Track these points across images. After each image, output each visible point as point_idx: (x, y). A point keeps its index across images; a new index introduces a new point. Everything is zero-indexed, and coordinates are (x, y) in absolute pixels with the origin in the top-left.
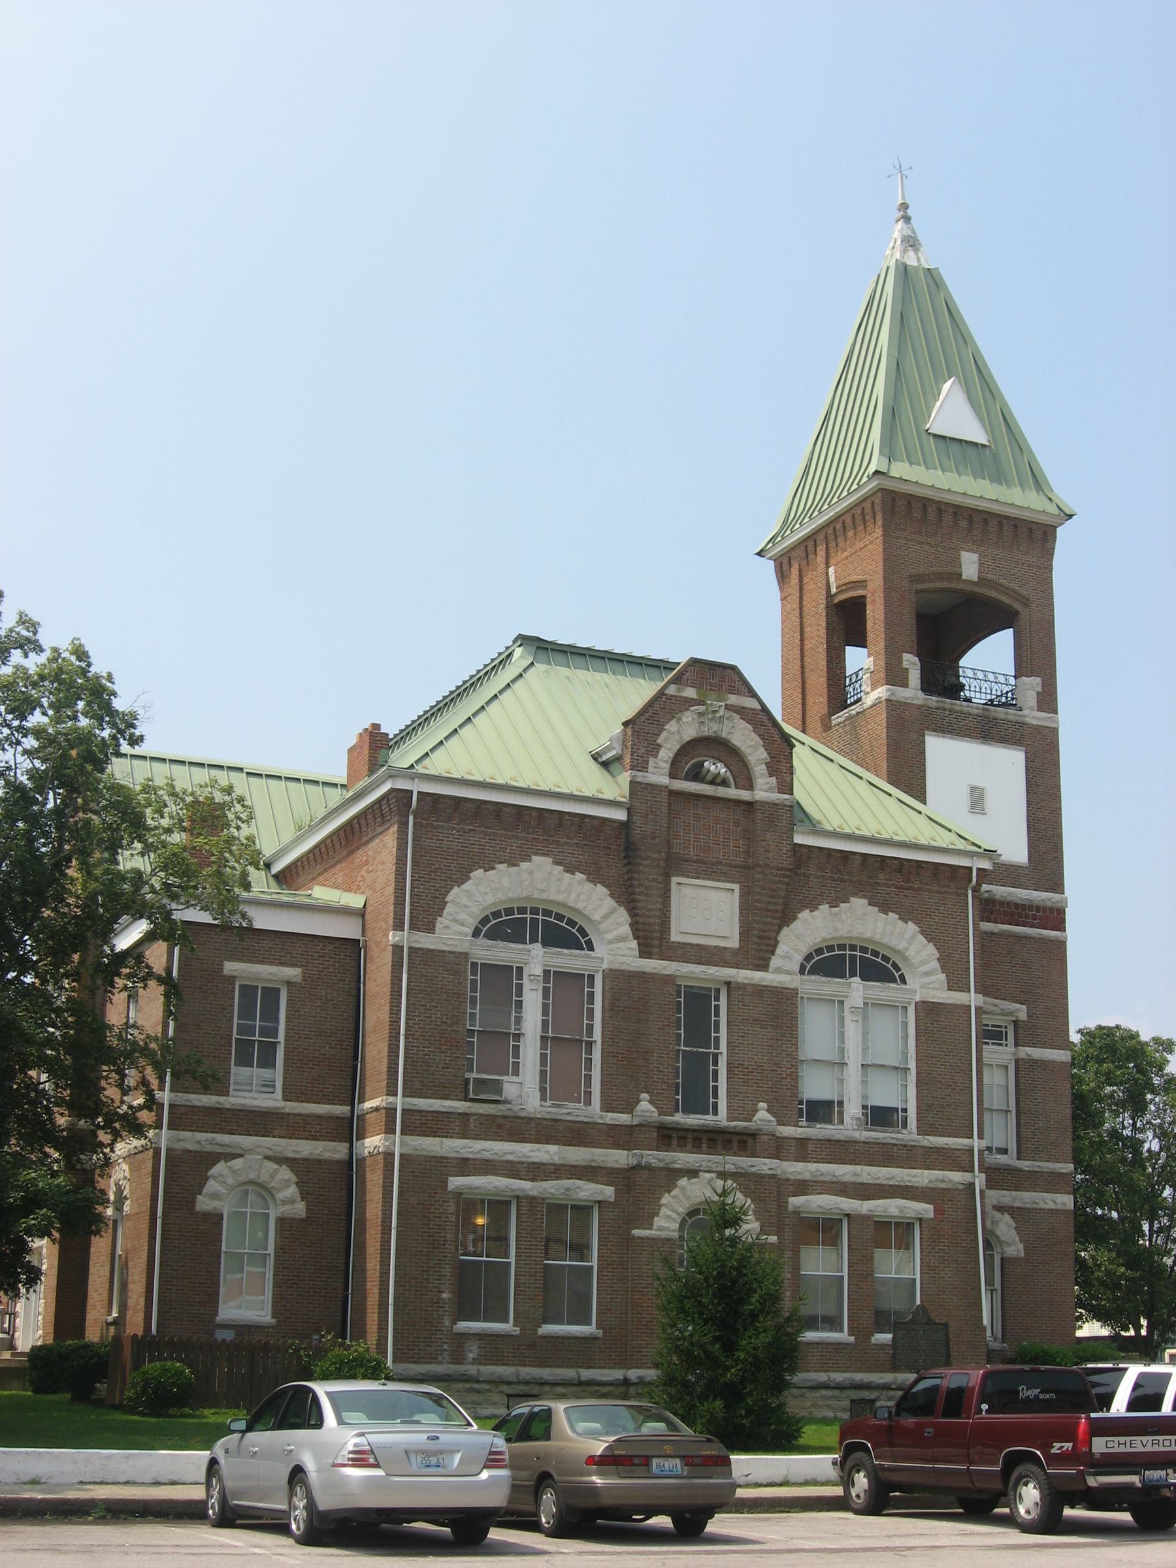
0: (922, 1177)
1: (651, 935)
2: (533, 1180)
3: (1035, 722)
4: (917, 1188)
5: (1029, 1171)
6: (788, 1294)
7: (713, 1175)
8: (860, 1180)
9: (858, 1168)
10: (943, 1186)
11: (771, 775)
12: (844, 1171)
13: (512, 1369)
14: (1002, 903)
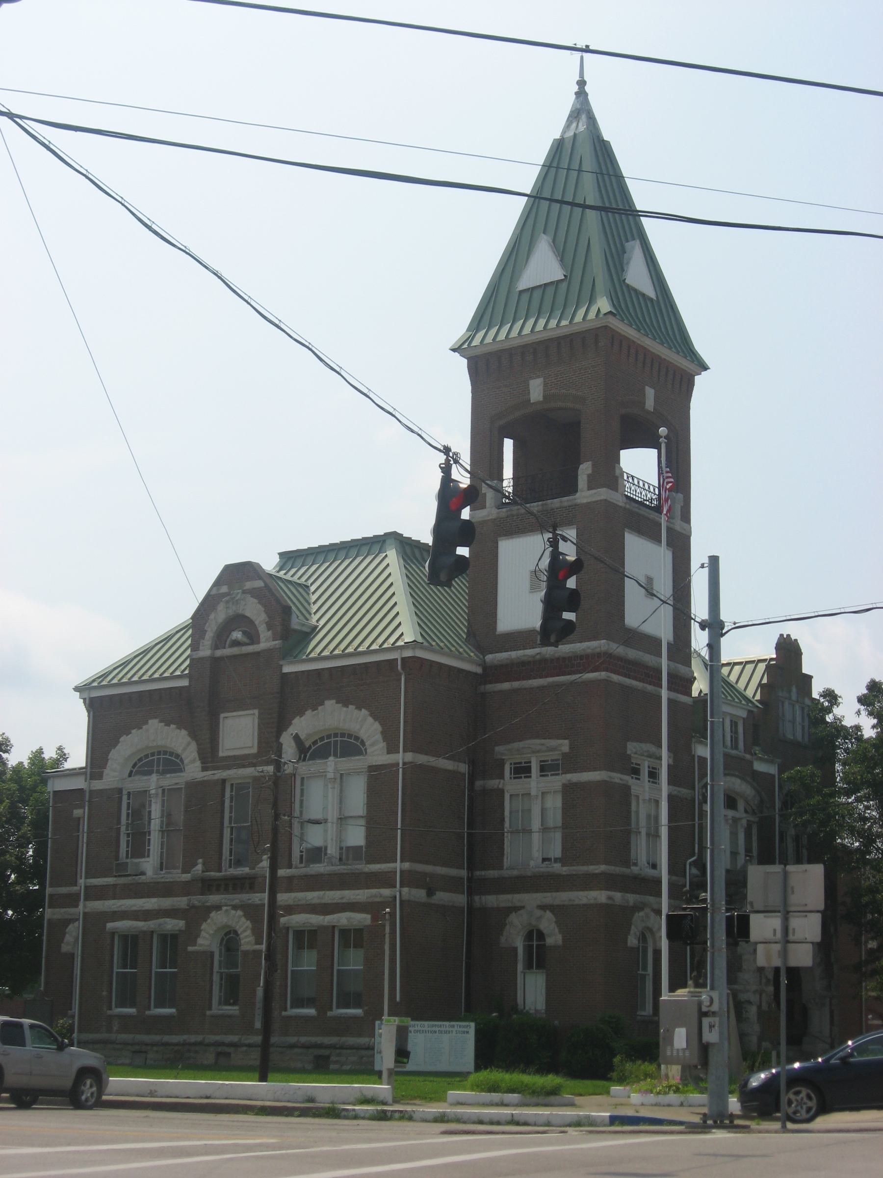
0: (361, 895)
1: (209, 755)
2: (145, 921)
3: (585, 501)
4: (360, 903)
5: (568, 875)
6: (278, 983)
7: (228, 908)
8: (323, 901)
9: (322, 893)
10: (378, 900)
11: (269, 630)
12: (312, 896)
13: (132, 1036)
14: (552, 660)
